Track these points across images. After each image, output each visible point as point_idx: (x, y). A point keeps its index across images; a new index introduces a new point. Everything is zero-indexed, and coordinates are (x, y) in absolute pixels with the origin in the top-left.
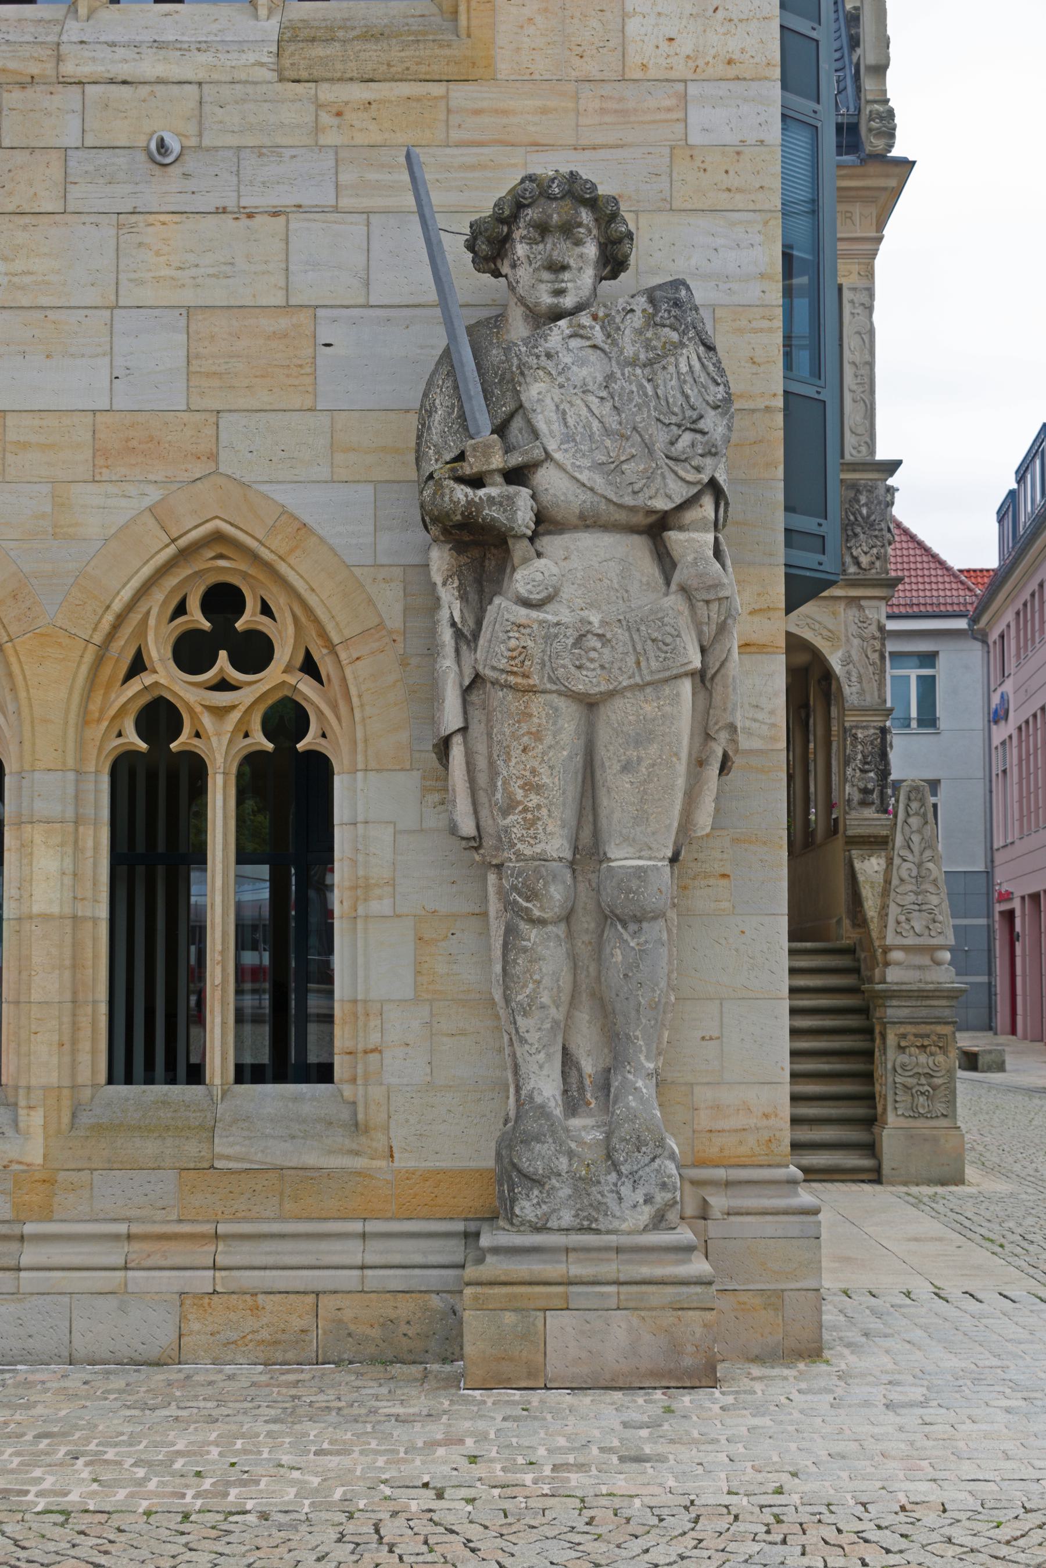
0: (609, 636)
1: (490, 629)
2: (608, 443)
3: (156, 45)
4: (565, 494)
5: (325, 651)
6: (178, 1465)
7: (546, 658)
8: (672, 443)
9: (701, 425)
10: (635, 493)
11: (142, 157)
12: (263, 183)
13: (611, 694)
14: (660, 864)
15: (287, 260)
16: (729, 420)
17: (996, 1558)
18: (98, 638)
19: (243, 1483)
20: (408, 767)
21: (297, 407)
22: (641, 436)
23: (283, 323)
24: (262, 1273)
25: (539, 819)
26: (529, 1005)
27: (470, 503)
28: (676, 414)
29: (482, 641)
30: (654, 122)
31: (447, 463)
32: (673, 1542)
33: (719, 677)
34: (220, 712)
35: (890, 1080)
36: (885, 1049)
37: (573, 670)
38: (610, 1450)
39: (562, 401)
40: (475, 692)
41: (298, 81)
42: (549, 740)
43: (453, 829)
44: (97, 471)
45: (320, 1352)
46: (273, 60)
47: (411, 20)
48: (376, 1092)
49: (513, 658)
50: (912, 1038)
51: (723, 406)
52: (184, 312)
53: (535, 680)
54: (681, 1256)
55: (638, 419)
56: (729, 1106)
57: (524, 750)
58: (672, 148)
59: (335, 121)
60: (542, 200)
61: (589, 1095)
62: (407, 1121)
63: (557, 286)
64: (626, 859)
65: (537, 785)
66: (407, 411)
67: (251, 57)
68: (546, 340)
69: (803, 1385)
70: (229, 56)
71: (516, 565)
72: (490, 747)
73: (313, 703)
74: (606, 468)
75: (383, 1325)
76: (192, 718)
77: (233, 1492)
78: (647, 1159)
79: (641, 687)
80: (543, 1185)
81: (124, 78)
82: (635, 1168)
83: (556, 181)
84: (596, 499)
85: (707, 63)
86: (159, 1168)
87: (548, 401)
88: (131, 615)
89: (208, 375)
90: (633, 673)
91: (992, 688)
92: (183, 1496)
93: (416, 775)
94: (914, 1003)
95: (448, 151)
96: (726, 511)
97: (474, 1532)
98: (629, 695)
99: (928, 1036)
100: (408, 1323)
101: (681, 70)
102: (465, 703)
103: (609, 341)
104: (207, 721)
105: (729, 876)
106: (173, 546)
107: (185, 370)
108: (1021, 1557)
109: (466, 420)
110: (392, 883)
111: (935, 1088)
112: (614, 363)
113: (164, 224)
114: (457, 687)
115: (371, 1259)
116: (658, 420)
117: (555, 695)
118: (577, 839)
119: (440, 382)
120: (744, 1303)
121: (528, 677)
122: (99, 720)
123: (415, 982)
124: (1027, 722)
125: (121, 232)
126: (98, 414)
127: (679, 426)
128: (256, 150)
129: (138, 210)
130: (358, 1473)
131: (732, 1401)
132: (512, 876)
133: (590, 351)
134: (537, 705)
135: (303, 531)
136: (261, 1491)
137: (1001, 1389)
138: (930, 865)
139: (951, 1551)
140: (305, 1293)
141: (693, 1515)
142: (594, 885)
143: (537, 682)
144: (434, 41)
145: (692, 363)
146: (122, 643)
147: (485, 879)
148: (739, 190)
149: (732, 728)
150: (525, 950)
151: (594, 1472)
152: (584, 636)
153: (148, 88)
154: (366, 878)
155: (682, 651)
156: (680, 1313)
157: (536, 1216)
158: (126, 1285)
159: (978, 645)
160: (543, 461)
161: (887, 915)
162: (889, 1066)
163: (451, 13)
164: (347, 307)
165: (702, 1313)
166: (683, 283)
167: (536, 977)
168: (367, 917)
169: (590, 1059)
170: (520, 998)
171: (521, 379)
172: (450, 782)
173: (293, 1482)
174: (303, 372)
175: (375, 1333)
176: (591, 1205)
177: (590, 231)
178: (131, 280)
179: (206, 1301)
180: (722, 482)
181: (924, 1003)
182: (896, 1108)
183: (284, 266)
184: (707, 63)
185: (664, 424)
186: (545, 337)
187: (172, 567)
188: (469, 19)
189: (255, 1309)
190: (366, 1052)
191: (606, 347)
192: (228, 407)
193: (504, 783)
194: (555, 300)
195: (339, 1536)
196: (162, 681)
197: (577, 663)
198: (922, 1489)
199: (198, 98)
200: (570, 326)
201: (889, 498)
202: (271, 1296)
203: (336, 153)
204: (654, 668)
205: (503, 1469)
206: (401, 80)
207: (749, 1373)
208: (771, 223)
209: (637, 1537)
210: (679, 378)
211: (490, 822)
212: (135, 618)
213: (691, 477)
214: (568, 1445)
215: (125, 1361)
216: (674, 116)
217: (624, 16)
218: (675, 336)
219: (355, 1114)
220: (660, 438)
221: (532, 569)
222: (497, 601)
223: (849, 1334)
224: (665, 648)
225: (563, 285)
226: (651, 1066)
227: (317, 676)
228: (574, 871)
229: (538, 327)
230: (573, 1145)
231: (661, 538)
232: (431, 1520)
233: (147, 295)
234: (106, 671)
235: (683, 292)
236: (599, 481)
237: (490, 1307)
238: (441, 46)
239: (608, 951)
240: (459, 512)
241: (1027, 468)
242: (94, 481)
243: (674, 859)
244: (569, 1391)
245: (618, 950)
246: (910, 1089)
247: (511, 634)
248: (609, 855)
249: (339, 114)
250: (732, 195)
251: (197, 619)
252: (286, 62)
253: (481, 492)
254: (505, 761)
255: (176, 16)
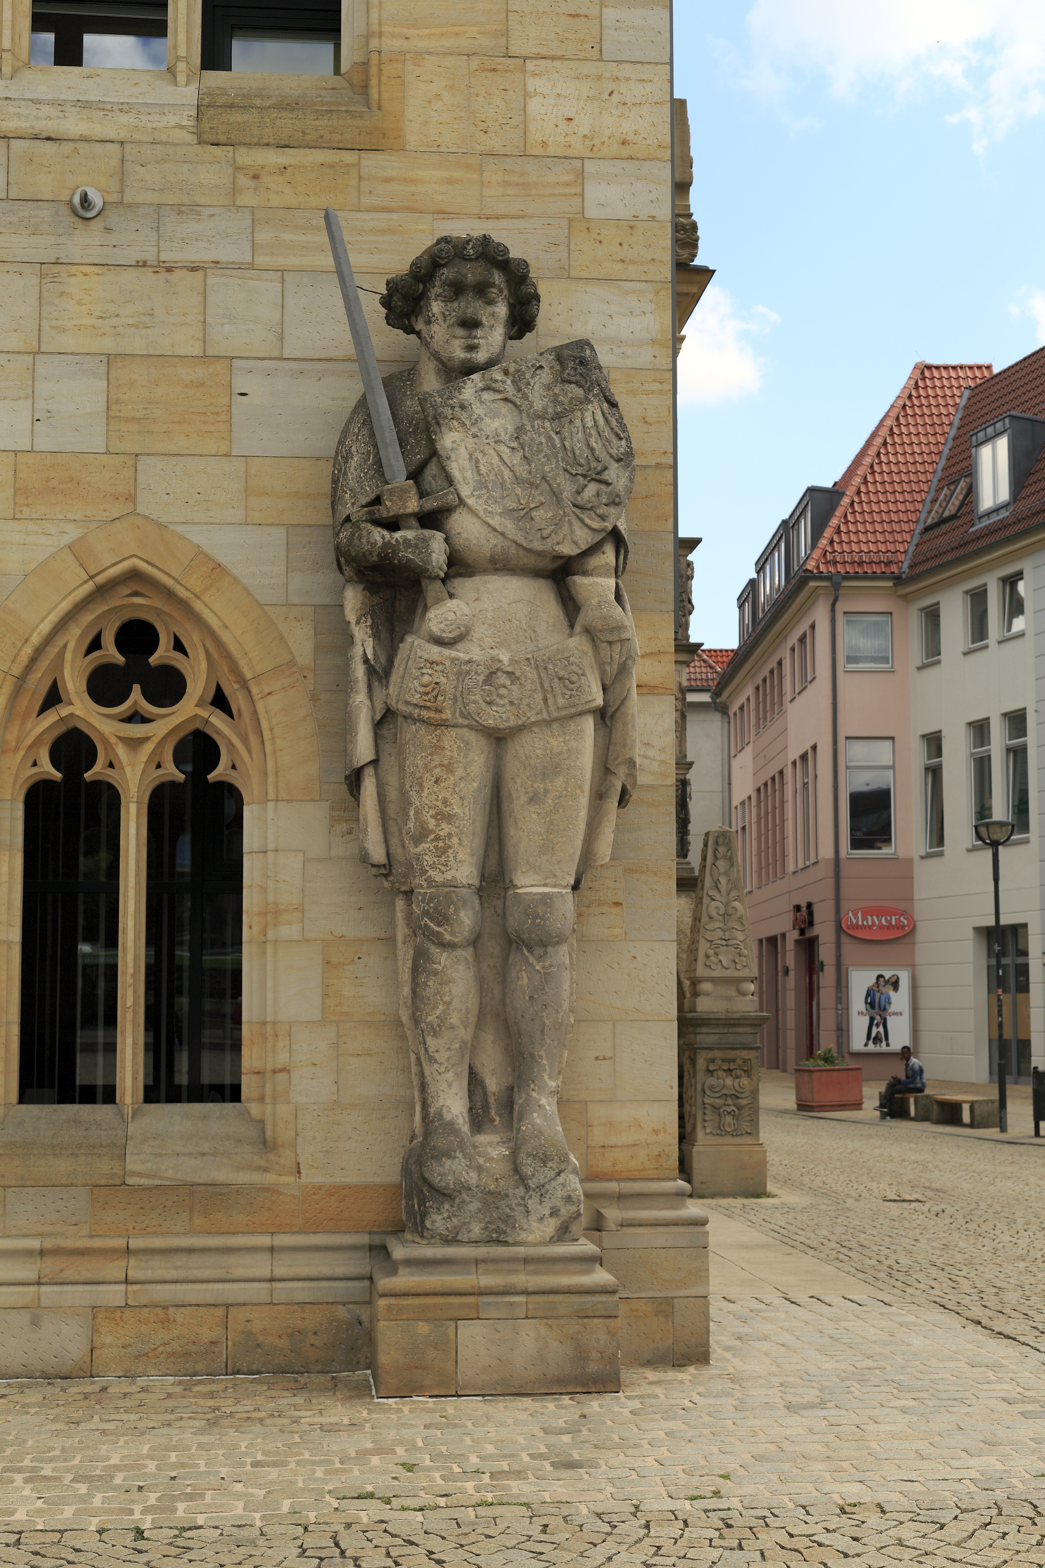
0: (518, 674)
1: (403, 666)
2: (518, 491)
3: (79, 104)
4: (477, 538)
5: (236, 686)
6: (118, 1480)
7: (458, 694)
8: (578, 493)
9: (605, 476)
10: (543, 538)
11: (66, 210)
12: (182, 239)
13: (520, 729)
14: (564, 891)
15: (205, 313)
16: (631, 472)
17: (954, 1561)
18: (17, 670)
19: (190, 1497)
20: (317, 798)
21: (213, 452)
22: (549, 485)
23: (201, 372)
24: (172, 1287)
25: (450, 847)
26: (439, 1026)
27: (386, 545)
28: (581, 466)
29: (394, 678)
30: (554, 195)
31: (364, 507)
32: (633, 1549)
33: (618, 714)
34: (134, 744)
35: (699, 1101)
36: (695, 1072)
37: (484, 705)
38: (541, 1456)
39: (475, 450)
40: (386, 726)
41: (217, 145)
42: (460, 772)
43: (364, 858)
44: (17, 509)
45: (229, 1363)
46: (192, 123)
47: (323, 93)
48: (283, 1110)
49: (427, 694)
50: (720, 1062)
51: (625, 459)
52: (104, 358)
53: (447, 715)
54: (585, 1266)
55: (547, 468)
56: (621, 1123)
57: (436, 782)
58: (570, 220)
59: (251, 183)
60: (457, 260)
61: (493, 1113)
62: (314, 1138)
63: (470, 342)
64: (532, 886)
65: (449, 815)
66: (319, 459)
67: (172, 120)
68: (460, 393)
69: (701, 1389)
70: (150, 118)
71: (429, 604)
72: (402, 778)
73: (224, 736)
74: (516, 514)
75: (291, 1336)
76: (106, 749)
77: (181, 1507)
78: (552, 1174)
79: (548, 723)
80: (453, 1200)
81: (49, 134)
82: (542, 1182)
83: (471, 244)
84: (507, 543)
85: (603, 143)
86: (72, 1185)
87: (462, 450)
88: (48, 649)
89: (128, 420)
90: (541, 710)
91: (732, 754)
92: (131, 1512)
93: (325, 805)
94: (722, 1031)
95: (359, 215)
96: (625, 558)
97: (433, 1543)
98: (536, 730)
99: (734, 1060)
100: (315, 1333)
101: (579, 148)
102: (377, 738)
103: (520, 395)
104: (121, 751)
105: (621, 904)
106: (91, 583)
107: (105, 414)
108: (975, 1559)
109: (381, 466)
110: (301, 909)
111: (740, 1108)
112: (524, 415)
113: (86, 275)
114: (369, 721)
115: (279, 1272)
116: (566, 470)
117: (466, 729)
118: (483, 867)
119: (356, 430)
120: (637, 1311)
121: (441, 712)
122: (16, 750)
123: (323, 1004)
124: (766, 784)
125: (44, 281)
126: (19, 454)
127: (585, 476)
128: (175, 208)
129: (61, 261)
130: (300, 1485)
131: (640, 1406)
132: (423, 901)
133: (502, 403)
134: (450, 738)
135: (217, 571)
136: (206, 1505)
137: (888, 1389)
138: (737, 904)
139: (907, 1554)
140: (215, 1305)
141: (643, 1522)
142: (499, 911)
143: (449, 716)
144: (346, 112)
145: (597, 418)
146: (39, 675)
147: (393, 905)
148: (632, 262)
149: (631, 763)
150: (436, 973)
151: (532, 1479)
152: (495, 673)
153: (71, 145)
154: (276, 904)
155: (587, 689)
156: (585, 1320)
157: (447, 1229)
158: (39, 1300)
159: (717, 716)
160: (456, 507)
161: (697, 949)
162: (699, 1088)
163: (362, 87)
164: (262, 359)
165: (607, 1321)
166: (588, 343)
167: (446, 999)
168: (276, 941)
169: (494, 1078)
170: (430, 1019)
171: (438, 429)
172: (361, 812)
173: (238, 1496)
174: (219, 419)
175: (284, 1343)
176: (500, 1218)
177: (501, 291)
178: (53, 328)
179: (118, 1314)
180: (623, 532)
181: (731, 1030)
182: (705, 1127)
183: (202, 319)
184: (603, 143)
185: (571, 474)
186: (459, 390)
187: (88, 603)
188: (379, 92)
189: (166, 1322)
190: (274, 1072)
191: (517, 401)
192: (146, 451)
193: (417, 813)
194: (468, 355)
195: (300, 1550)
196: (78, 713)
197: (488, 699)
198: (853, 1491)
199: (120, 156)
200: (483, 379)
201: (689, 573)
202: (182, 1310)
203: (253, 214)
204: (560, 705)
205: (443, 1477)
206: (315, 148)
207: (646, 1378)
208: (662, 293)
209: (595, 1545)
210: (585, 432)
211: (400, 850)
212: (52, 651)
213: (596, 525)
214: (497, 1452)
215: (37, 1374)
216: (573, 190)
217: (526, 95)
218: (579, 392)
219: (263, 1131)
220: (567, 488)
221: (445, 609)
222: (409, 639)
223: (723, 1338)
224: (571, 686)
225: (476, 341)
226: (554, 1084)
227: (184, 652)
228: (481, 897)
229: (450, 381)
230: (481, 1161)
231: (564, 582)
232: (385, 1531)
233: (70, 342)
234: (24, 702)
235: (588, 352)
236: (509, 526)
237: (404, 1317)
238: (353, 117)
239: (514, 974)
240: (375, 553)
241: (766, 560)
242: (14, 519)
243: (575, 887)
244: (480, 1398)
245: (524, 974)
246: (718, 1109)
247: (424, 671)
248: (516, 882)
249: (256, 177)
250: (625, 266)
251: (111, 653)
252: (206, 126)
253: (398, 535)
254: (418, 792)
255: (96, 78)
